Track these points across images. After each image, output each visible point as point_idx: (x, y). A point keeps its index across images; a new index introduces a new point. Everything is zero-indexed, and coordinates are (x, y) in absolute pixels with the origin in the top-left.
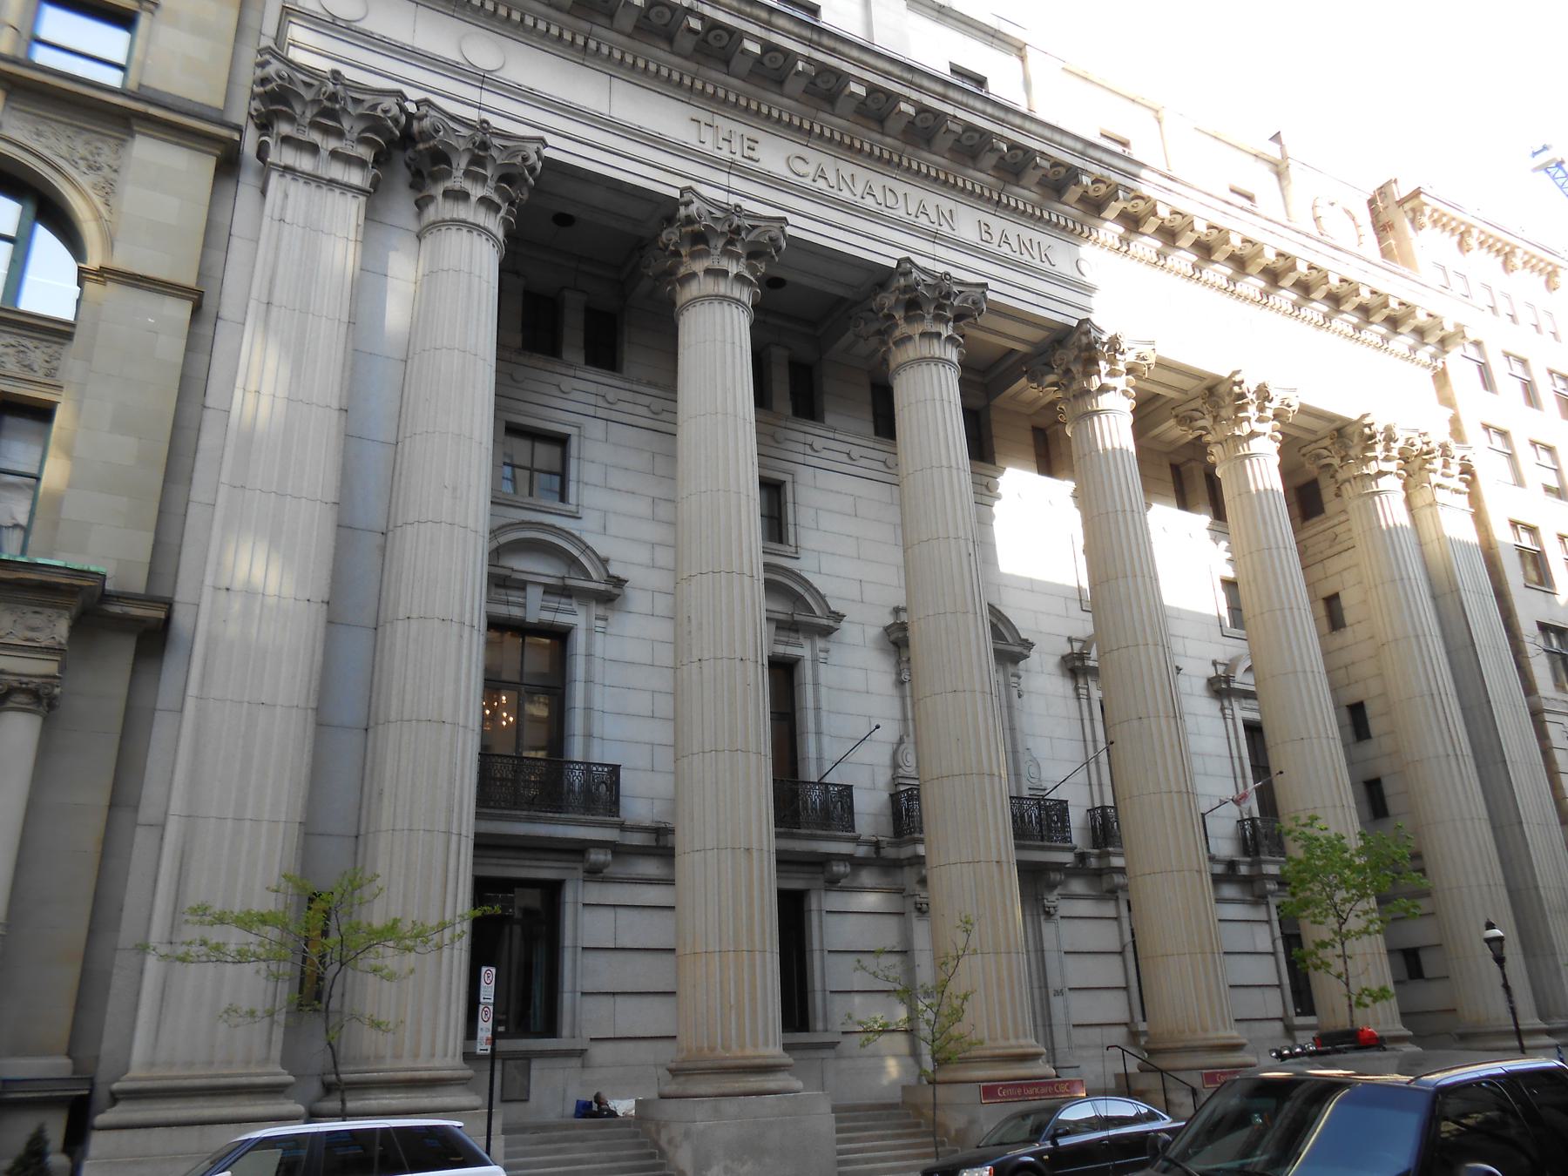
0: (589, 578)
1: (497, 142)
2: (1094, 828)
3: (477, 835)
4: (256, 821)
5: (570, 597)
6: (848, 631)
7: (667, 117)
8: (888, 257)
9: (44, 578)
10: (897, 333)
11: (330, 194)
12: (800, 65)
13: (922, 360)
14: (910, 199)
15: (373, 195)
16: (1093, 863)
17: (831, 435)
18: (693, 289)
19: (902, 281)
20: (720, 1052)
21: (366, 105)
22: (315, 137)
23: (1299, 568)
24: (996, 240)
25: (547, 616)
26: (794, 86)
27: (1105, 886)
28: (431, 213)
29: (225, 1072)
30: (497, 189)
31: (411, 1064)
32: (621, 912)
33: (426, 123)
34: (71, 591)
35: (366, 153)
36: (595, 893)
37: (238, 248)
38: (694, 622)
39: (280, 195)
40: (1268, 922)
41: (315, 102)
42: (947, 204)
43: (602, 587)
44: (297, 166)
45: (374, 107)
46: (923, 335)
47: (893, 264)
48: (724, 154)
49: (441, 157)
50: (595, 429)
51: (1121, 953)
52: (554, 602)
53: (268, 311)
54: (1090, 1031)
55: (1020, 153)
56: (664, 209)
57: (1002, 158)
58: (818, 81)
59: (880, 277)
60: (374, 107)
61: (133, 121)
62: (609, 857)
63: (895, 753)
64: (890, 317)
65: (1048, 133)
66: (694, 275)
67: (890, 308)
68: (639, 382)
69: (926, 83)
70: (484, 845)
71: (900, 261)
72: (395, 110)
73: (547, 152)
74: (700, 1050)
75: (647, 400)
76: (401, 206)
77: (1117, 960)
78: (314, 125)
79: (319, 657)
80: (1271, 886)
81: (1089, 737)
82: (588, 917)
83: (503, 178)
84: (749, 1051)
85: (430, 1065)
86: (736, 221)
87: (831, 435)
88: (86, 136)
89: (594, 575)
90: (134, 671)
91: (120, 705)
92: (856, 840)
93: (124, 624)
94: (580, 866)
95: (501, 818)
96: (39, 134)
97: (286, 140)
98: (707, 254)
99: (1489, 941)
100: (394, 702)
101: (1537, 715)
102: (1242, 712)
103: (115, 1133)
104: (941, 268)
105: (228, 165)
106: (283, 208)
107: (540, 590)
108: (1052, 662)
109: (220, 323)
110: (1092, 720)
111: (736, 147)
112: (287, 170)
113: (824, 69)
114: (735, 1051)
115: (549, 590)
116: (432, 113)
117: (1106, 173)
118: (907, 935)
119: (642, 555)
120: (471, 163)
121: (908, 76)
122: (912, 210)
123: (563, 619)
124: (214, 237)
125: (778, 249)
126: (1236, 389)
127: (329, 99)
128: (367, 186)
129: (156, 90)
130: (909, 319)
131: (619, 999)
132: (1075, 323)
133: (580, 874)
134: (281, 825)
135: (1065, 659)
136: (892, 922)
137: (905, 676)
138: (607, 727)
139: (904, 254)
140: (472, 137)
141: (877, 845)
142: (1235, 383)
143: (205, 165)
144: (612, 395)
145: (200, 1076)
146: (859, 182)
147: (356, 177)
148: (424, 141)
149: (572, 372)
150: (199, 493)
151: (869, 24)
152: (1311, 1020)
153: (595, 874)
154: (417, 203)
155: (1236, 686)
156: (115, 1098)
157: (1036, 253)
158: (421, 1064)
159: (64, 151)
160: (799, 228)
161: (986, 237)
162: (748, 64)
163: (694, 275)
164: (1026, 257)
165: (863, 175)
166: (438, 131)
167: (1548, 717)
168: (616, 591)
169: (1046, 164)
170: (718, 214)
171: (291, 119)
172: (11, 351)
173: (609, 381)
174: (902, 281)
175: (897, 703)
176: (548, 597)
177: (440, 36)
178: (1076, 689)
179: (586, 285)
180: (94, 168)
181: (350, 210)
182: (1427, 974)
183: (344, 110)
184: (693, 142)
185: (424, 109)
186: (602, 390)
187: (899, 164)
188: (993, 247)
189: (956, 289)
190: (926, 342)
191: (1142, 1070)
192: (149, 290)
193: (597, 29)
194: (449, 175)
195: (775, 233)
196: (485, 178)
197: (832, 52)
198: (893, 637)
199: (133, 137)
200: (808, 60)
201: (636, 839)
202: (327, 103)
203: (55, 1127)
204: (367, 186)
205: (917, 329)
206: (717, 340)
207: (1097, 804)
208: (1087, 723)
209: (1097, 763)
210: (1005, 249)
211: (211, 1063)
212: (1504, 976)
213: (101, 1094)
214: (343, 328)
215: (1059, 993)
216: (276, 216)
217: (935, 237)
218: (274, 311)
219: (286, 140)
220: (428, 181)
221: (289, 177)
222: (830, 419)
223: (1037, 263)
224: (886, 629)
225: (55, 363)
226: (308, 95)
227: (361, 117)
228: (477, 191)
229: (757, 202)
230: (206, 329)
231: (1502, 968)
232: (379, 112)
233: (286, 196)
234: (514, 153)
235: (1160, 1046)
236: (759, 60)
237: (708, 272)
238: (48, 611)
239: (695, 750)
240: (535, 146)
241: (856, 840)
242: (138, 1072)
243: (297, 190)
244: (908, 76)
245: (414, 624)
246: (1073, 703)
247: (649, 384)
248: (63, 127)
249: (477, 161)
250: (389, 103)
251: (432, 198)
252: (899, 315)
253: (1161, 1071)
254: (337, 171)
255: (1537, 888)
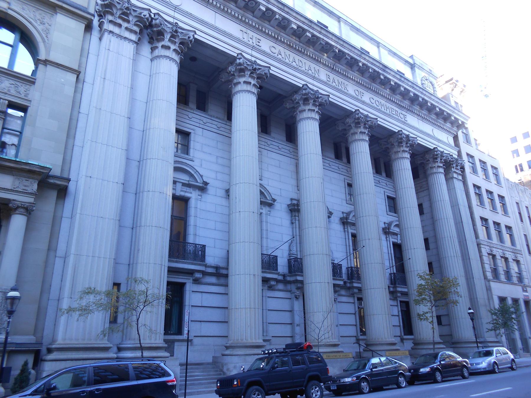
0: (197, 182)
1: (180, 30)
2: (348, 274)
3: (169, 267)
4: (99, 257)
5: (190, 187)
6: (277, 205)
7: (233, 28)
8: (396, 129)
9: (31, 168)
10: (300, 109)
11: (113, 37)
12: (277, 16)
13: (308, 118)
14: (307, 64)
15: (138, 43)
16: (348, 285)
17: (273, 140)
18: (239, 88)
19: (304, 91)
20: (244, 341)
21: (138, 12)
22: (120, 21)
23: (450, 206)
24: (331, 81)
25: (182, 194)
26: (367, 75)
27: (351, 292)
28: (157, 52)
29: (101, 342)
30: (179, 47)
31: (149, 342)
32: (204, 294)
33: (158, 21)
34: (39, 173)
35: (137, 29)
36: (196, 288)
37: (92, 58)
38: (238, 199)
39: (108, 41)
40: (397, 306)
41: (121, 9)
42: (317, 68)
43: (201, 185)
44: (114, 31)
45: (141, 13)
46: (309, 110)
47: (301, 86)
48: (250, 43)
49: (160, 34)
50: (199, 131)
51: (355, 314)
52: (185, 189)
53: (104, 81)
54: (345, 338)
55: (315, 38)
56: (232, 60)
57: (335, 54)
58: (282, 23)
59: (296, 89)
60: (141, 13)
61: (57, 8)
62: (201, 276)
63: (290, 246)
64: (298, 103)
65: (350, 48)
66: (240, 83)
67: (298, 100)
68: (214, 117)
69: (331, 36)
70: (171, 271)
71: (303, 85)
72: (148, 16)
73: (196, 36)
74: (238, 340)
75: (216, 123)
76: (146, 49)
77: (354, 316)
78: (120, 17)
79: (120, 203)
80: (399, 295)
81: (348, 244)
82: (194, 295)
83: (180, 43)
84: (254, 341)
85: (155, 342)
86: (255, 66)
87: (273, 140)
88: (40, 12)
89: (199, 181)
90: (56, 204)
91: (52, 214)
92: (278, 274)
93: (54, 186)
94: (191, 278)
95: (176, 262)
96: (23, 9)
97: (111, 22)
98: (244, 76)
99: (469, 313)
100: (143, 219)
101: (479, 245)
102: (392, 239)
103: (54, 362)
104: (315, 89)
105: (89, 28)
106: (109, 45)
107: (181, 184)
108: (284, 207)
109: (85, 83)
110: (349, 239)
111: (254, 42)
112: (111, 32)
113: (284, 18)
114: (249, 341)
115: (184, 185)
116: (160, 18)
117: (366, 63)
118: (292, 306)
119: (213, 175)
120: (171, 37)
121: (310, 24)
122: (307, 68)
123: (188, 195)
124: (84, 53)
125: (267, 77)
126: (400, 136)
127: (126, 9)
128: (137, 41)
129: (80, 5)
130: (304, 104)
131: (203, 323)
132: (354, 110)
133: (191, 281)
134: (108, 259)
135: (341, 219)
136: (287, 301)
137: (294, 221)
138: (201, 232)
139: (240, 52)
140: (172, 28)
141: (284, 276)
142: (400, 134)
143: (82, 26)
144: (205, 120)
145: (81, 343)
146: (292, 57)
147: (133, 37)
148: (156, 27)
149: (192, 111)
150: (78, 141)
151: (294, 4)
152: (412, 337)
153: (196, 281)
154: (151, 49)
155: (391, 231)
156: (50, 351)
157: (343, 87)
158: (153, 341)
159: (32, 16)
160: (274, 71)
161: (328, 79)
162: (260, 14)
163: (240, 83)
164: (340, 87)
165: (292, 55)
166: (161, 25)
167: (482, 246)
168: (205, 187)
169: (349, 58)
170: (249, 63)
171: (112, 14)
172: (13, 86)
173: (201, 114)
174: (304, 91)
175: (291, 229)
176: (183, 187)
177: (207, 15)
178: (344, 229)
179: (204, 82)
180: (43, 23)
181: (129, 48)
182: (443, 324)
183: (130, 13)
184: (241, 38)
185: (157, 17)
186: (202, 118)
187: (304, 53)
188: (331, 83)
189: (320, 96)
190: (310, 112)
191: (364, 350)
192: (62, 69)
193: (246, 14)
194: (163, 40)
195: (267, 71)
196: (175, 43)
197: (287, 13)
198: (290, 208)
199: (56, 14)
200: (280, 15)
201: (210, 270)
202: (125, 10)
203: (31, 360)
204: (137, 41)
205: (307, 108)
206: (245, 106)
207: (349, 266)
208: (347, 240)
209: (350, 253)
210: (334, 84)
211: (84, 340)
212: (473, 324)
213: (44, 350)
214: (129, 89)
215: (297, 325)
216: (107, 48)
217: (314, 78)
218: (106, 81)
219: (111, 22)
220: (155, 41)
221: (111, 35)
222: (273, 134)
223: (343, 89)
224: (288, 205)
225: (28, 92)
226: (119, 7)
227: (136, 16)
228: (173, 47)
229: (262, 61)
230: (80, 85)
231: (473, 322)
232: (142, 16)
233: (110, 41)
234: (186, 35)
235: (371, 343)
236: (264, 13)
237: (245, 82)
238: (31, 180)
239: (237, 241)
240: (193, 33)
241: (278, 274)
242: (61, 340)
243: (114, 39)
244: (310, 24)
245: (151, 193)
246: (343, 233)
247: (217, 118)
248: (32, 8)
249: (173, 36)
250: (146, 13)
251: (157, 47)
252: (301, 102)
253: (372, 351)
254: (127, 34)
255: (477, 298)
